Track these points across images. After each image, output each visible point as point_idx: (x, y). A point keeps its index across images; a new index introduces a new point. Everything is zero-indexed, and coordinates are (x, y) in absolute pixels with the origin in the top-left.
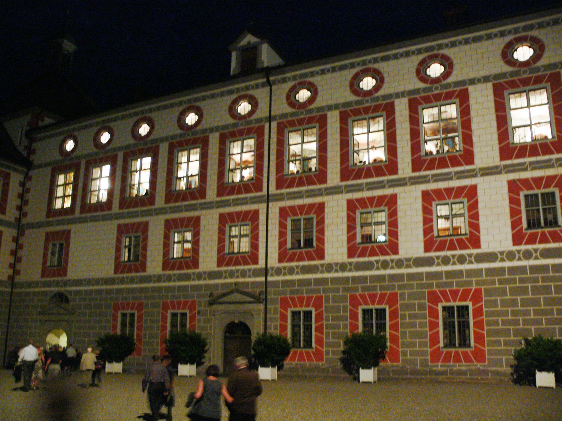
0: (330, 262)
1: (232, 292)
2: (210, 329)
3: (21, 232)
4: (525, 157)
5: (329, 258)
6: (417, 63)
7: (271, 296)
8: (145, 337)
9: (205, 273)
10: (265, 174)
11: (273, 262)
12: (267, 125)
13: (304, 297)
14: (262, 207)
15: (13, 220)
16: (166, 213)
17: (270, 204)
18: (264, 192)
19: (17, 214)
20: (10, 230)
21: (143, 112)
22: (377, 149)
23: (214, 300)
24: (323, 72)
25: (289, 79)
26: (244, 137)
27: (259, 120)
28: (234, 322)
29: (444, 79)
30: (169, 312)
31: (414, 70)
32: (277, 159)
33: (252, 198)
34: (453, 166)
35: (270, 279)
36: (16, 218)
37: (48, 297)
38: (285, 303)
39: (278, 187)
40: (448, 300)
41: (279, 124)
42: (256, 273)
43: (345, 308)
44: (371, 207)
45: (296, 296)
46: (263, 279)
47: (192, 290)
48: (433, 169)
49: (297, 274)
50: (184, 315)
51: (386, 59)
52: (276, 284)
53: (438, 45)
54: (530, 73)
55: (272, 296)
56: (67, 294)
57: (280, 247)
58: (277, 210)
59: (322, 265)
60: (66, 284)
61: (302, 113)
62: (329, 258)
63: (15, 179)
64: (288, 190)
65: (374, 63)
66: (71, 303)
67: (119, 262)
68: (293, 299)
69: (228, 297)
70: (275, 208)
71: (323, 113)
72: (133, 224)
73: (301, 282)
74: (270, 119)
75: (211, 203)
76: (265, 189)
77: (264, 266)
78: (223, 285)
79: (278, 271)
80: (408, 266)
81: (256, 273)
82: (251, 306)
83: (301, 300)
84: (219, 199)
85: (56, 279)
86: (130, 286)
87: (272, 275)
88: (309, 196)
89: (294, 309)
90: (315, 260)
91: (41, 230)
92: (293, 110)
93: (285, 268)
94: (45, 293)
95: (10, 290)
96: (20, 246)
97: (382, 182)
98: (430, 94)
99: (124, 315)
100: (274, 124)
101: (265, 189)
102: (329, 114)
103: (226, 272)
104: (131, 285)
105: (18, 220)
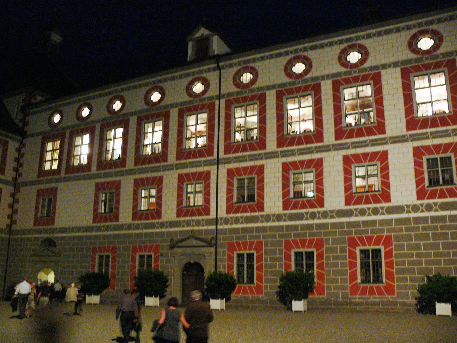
0: (268, 213)
1: (188, 238)
2: (171, 268)
3: (17, 189)
4: (427, 128)
5: (267, 210)
6: (339, 51)
7: (220, 242)
8: (118, 275)
9: (167, 222)
10: (216, 142)
11: (222, 213)
12: (217, 102)
13: (247, 242)
14: (213, 169)
15: (10, 179)
16: (135, 174)
17: (220, 166)
18: (215, 156)
19: (14, 174)
20: (8, 187)
21: (116, 91)
22: (307, 121)
23: (174, 245)
24: (262, 59)
25: (235, 64)
26: (198, 112)
27: (211, 98)
28: (190, 262)
29: (361, 65)
30: (138, 254)
31: (337, 57)
32: (225, 129)
33: (205, 161)
34: (368, 135)
35: (219, 227)
36: (13, 178)
37: (39, 242)
38: (231, 247)
39: (226, 152)
40: (364, 245)
41: (227, 101)
42: (208, 222)
43: (280, 251)
44: (302, 169)
45: (240, 241)
46: (214, 227)
47: (156, 237)
48: (352, 137)
49: (241, 223)
50: (149, 256)
51: (314, 48)
52: (224, 231)
53: (356, 37)
54: (431, 60)
55: (221, 241)
56: (55, 240)
57: (228, 202)
58: (226, 171)
59: (262, 216)
60: (53, 231)
61: (246, 92)
62: (267, 210)
63: (13, 146)
64: (234, 155)
65: (304, 51)
66: (58, 247)
67: (97, 214)
68: (238, 244)
69: (186, 242)
70: (224, 169)
71: (263, 92)
72: (108, 183)
73: (245, 230)
74: (219, 97)
75: (172, 165)
76: (215, 154)
77: (215, 217)
78: (181, 232)
79: (226, 221)
80: (332, 217)
81: (208, 222)
83: (245, 244)
84: (178, 162)
85: (45, 227)
86: (105, 233)
87: (221, 224)
88: (251, 160)
89: (239, 252)
90: (256, 211)
91: (34, 187)
92: (239, 90)
93: (231, 218)
94: (37, 239)
95: (8, 236)
96: (16, 201)
97: (311, 148)
98: (350, 76)
99: (101, 257)
100: (223, 101)
101: (215, 154)
102: (268, 93)
103: (184, 221)
104: (106, 232)
105: (15, 179)
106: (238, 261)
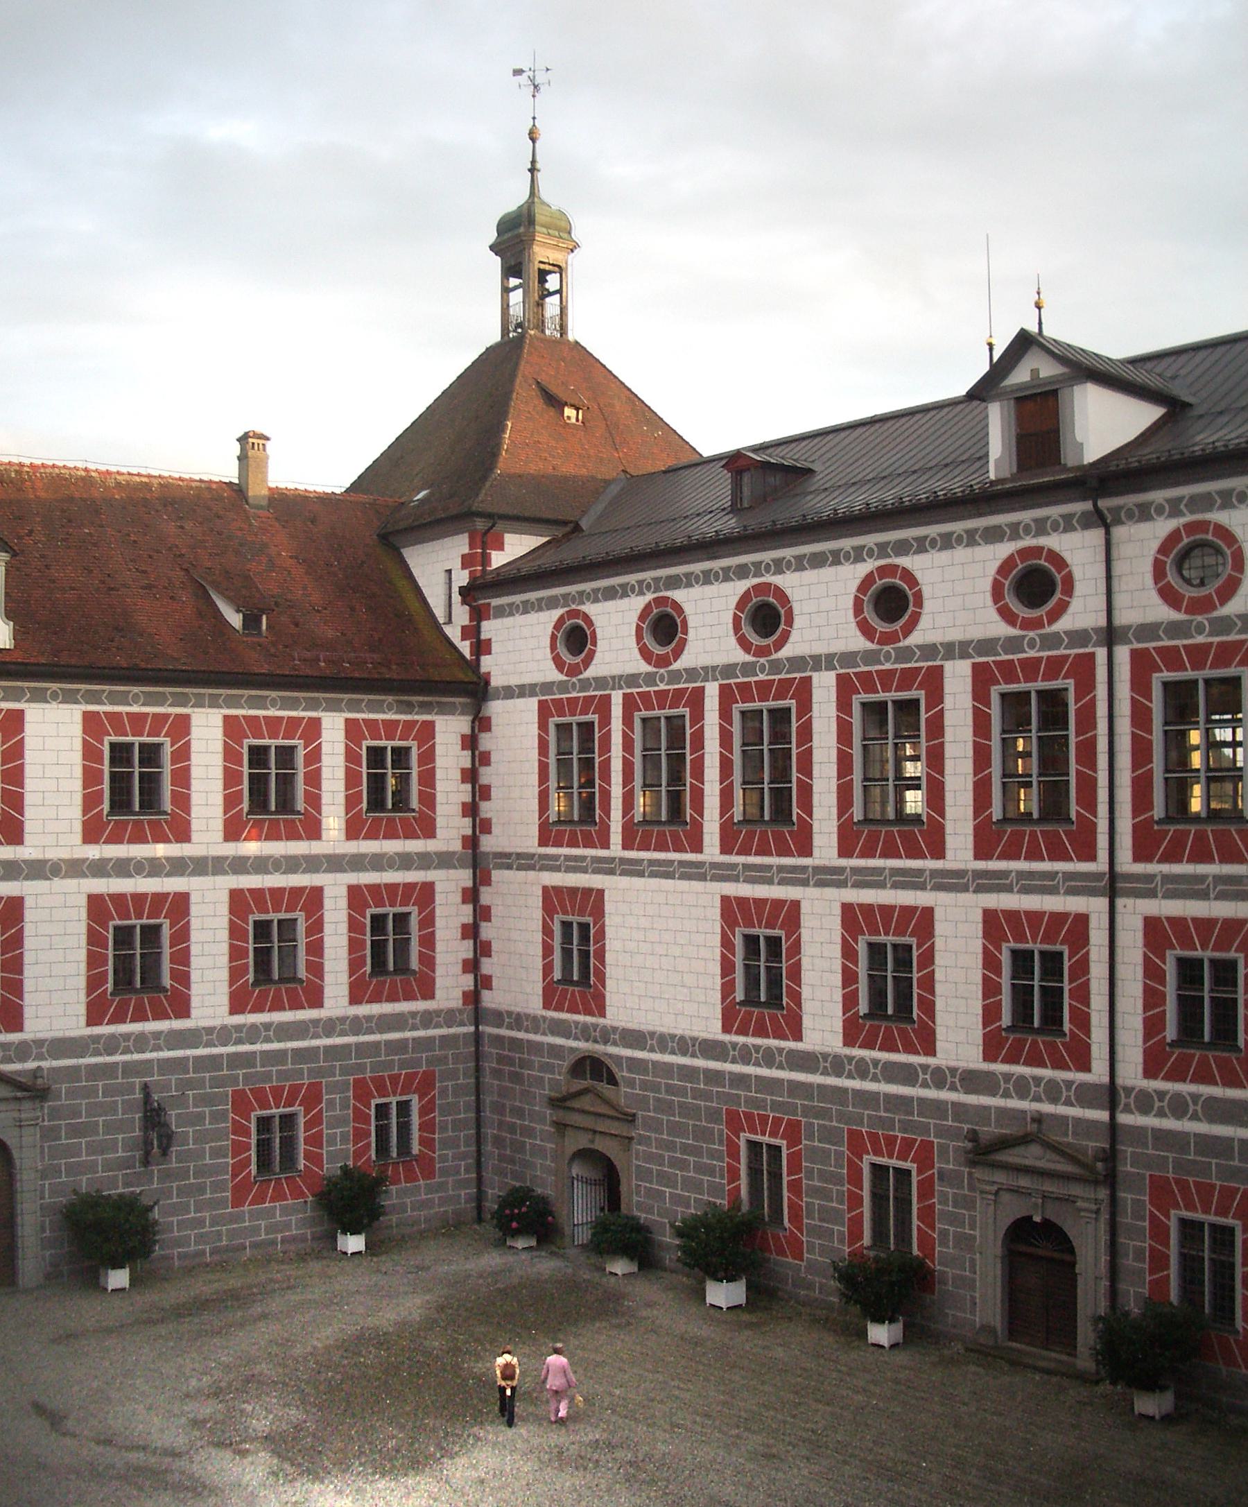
1: (1024, 1140)
2: (973, 1227)
3: (481, 878)
4: (1180, 861)
6: (1155, 545)
7: (1127, 1167)
8: (944, 1243)
9: (953, 1070)
10: (1103, 809)
11: (1131, 1072)
12: (1101, 654)
13: (1213, 1186)
15: (457, 846)
16: (1152, 894)
17: (1120, 902)
18: (1101, 865)
19: (465, 826)
20: (453, 873)
21: (758, 568)
23: (983, 1152)
24: (947, 542)
25: (1160, 510)
27: (1079, 637)
28: (1030, 1217)
29: (1051, 622)
31: (987, 584)
32: (1135, 767)
33: (1069, 876)
34: (779, 855)
37: (566, 1064)
38: (1161, 1192)
39: (1141, 854)
40: (1190, 1206)
41: (1135, 654)
42: (1085, 1095)
44: (1035, 942)
45: (1191, 1180)
46: (1103, 1116)
48: (1179, 860)
49: (876, 1078)
50: (904, 1174)
51: (800, 564)
53: (1221, 493)
54: (1210, 635)
55: (1129, 1168)
56: (608, 1061)
57: (1147, 1036)
58: (1139, 924)
60: (606, 1035)
61: (1200, 629)
63: (449, 729)
64: (1166, 868)
65: (1224, 506)
66: (624, 1089)
68: (1183, 1185)
69: (1019, 1150)
70: (1134, 912)
71: (935, 663)
72: (760, 903)
73: (1208, 1144)
74: (1111, 635)
75: (960, 874)
76: (1103, 854)
77: (1106, 1079)
78: (1002, 1112)
79: (1144, 1103)
81: (1085, 1095)
82: (1076, 1190)
83: (1205, 1191)
84: (981, 865)
86: (931, 1094)
87: (1127, 1110)
88: (1026, 890)
90: (1046, 1067)
91: (831, 892)
92: (869, 646)
93: (1161, 1095)
94: (555, 1051)
95: (472, 1029)
96: (482, 913)
97: (1201, 878)
98: (732, 681)
100: (1123, 654)
101: (1103, 854)
102: (949, 666)
103: (1007, 1077)
104: (758, 1066)
105: (471, 842)
106: (874, 1185)
